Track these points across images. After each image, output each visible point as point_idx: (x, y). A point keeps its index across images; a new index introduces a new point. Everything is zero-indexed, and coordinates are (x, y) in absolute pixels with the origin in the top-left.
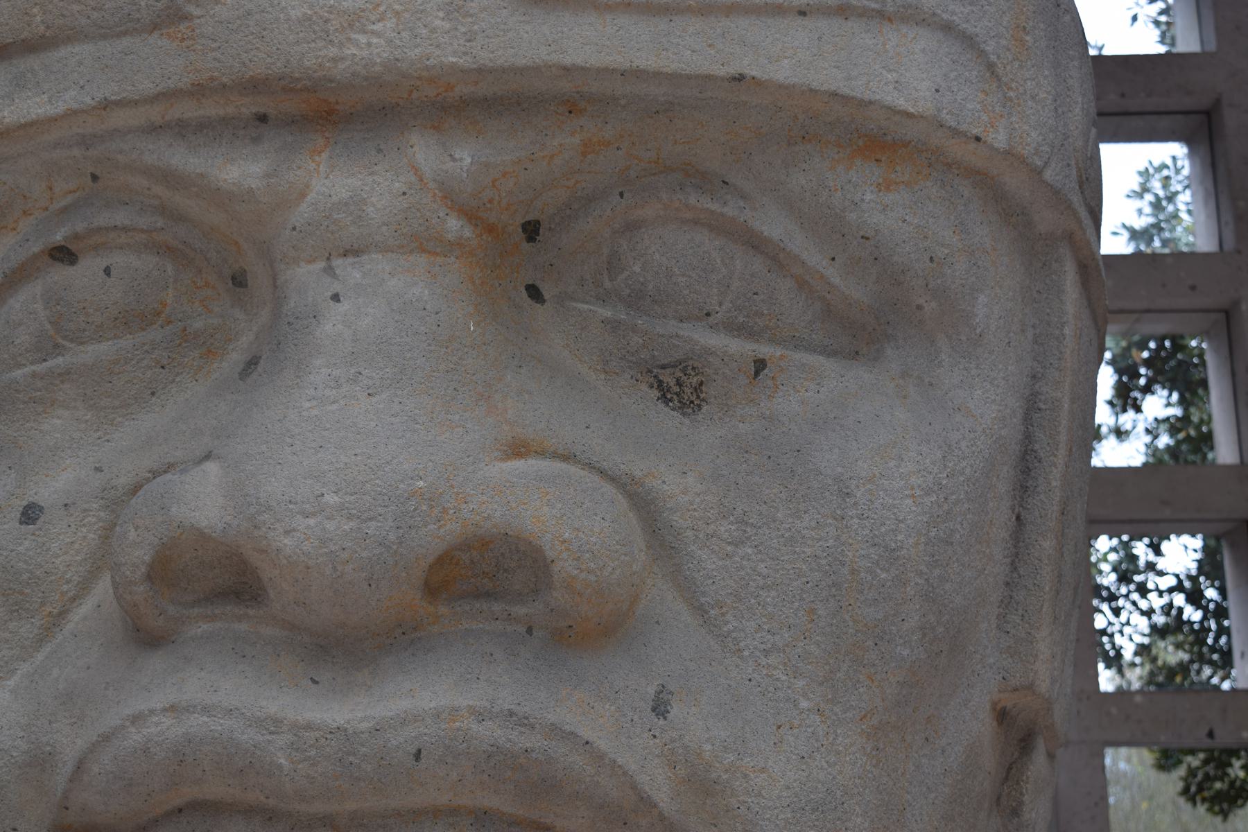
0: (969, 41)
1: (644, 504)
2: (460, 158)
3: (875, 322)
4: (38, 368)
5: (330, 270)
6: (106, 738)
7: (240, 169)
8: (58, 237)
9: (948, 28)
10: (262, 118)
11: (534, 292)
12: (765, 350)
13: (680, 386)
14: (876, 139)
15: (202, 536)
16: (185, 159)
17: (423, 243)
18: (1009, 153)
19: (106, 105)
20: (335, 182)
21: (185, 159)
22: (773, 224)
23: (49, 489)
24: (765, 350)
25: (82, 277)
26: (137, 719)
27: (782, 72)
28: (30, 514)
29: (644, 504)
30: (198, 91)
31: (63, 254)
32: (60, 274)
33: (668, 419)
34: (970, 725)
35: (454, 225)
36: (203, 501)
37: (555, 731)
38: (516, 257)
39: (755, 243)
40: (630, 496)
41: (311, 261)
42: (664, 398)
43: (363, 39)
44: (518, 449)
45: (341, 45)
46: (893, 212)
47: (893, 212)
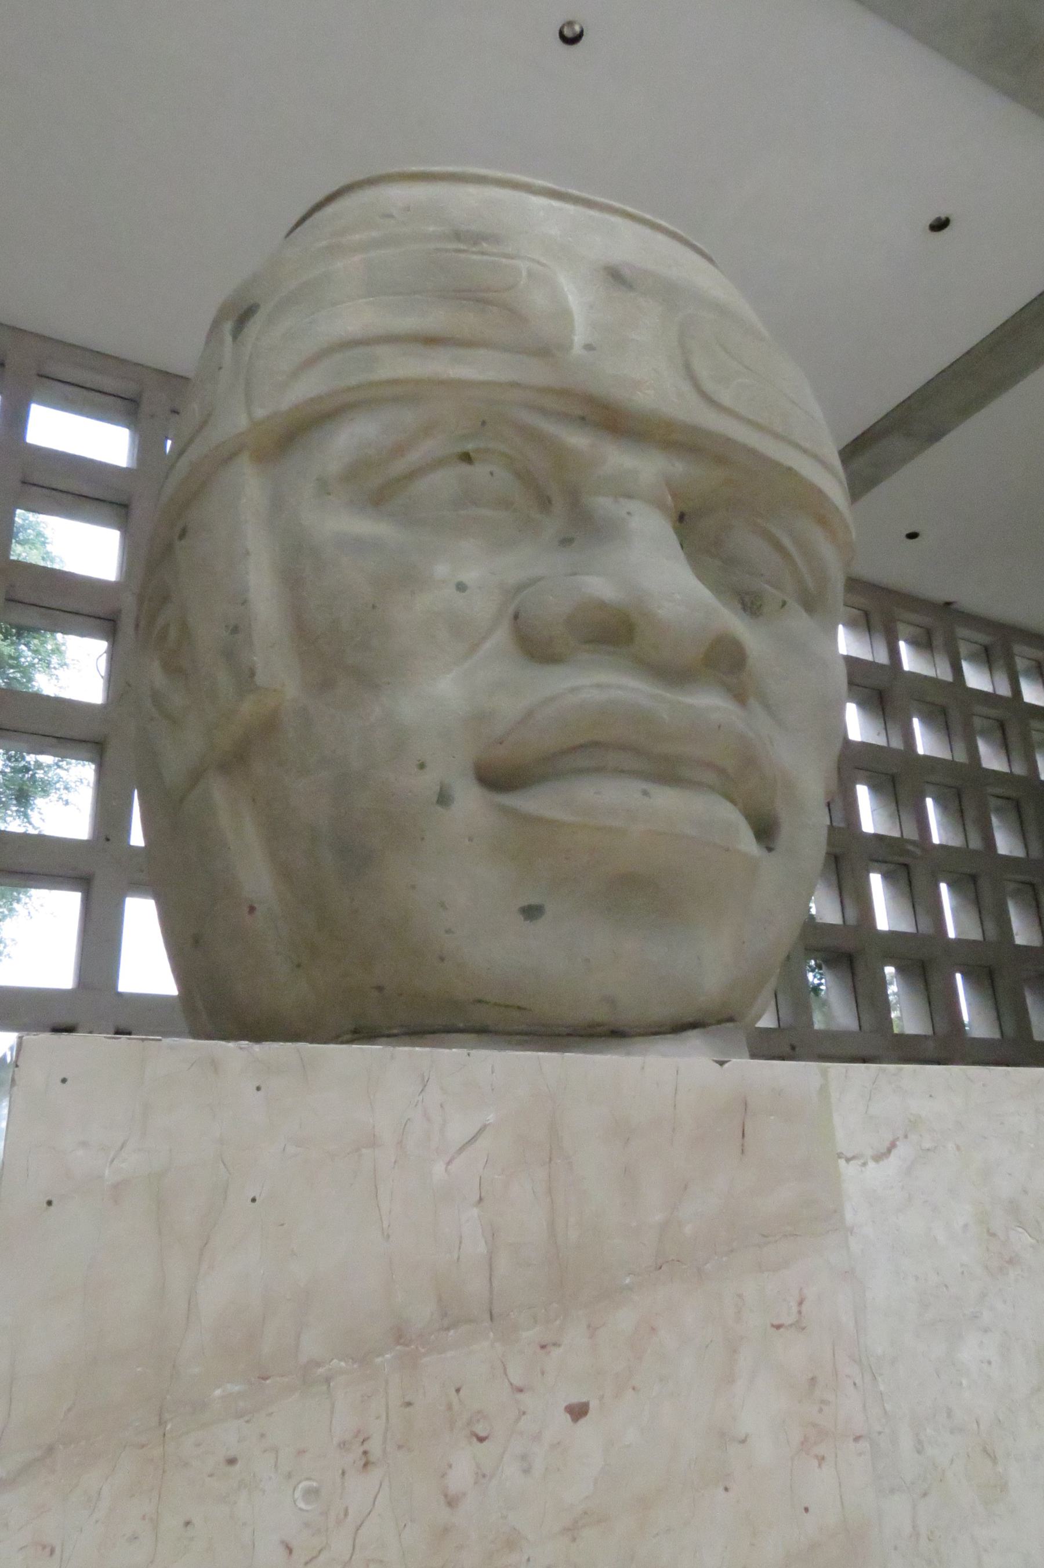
2: (679, 467)
8: (470, 447)
17: (661, 506)
20: (619, 459)
23: (470, 575)
25: (479, 471)
28: (461, 587)
31: (466, 458)
32: (464, 468)
36: (600, 587)
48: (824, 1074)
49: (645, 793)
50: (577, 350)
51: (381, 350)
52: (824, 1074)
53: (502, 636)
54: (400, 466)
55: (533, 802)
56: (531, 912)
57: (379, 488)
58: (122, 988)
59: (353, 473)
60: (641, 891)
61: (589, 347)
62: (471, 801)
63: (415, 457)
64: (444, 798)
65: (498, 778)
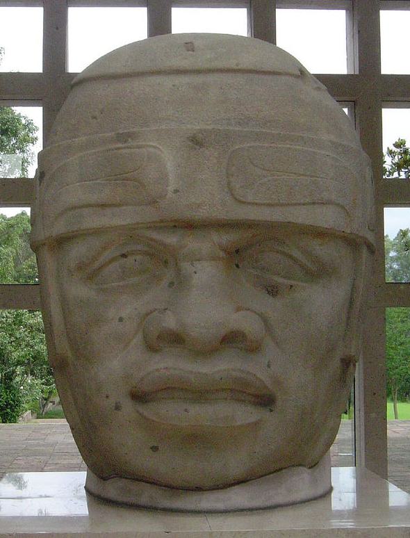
0: (343, 207)
1: (265, 320)
2: (227, 238)
3: (319, 272)
4: (121, 284)
5: (192, 264)
6: (149, 374)
7: (171, 239)
8: (124, 251)
9: (338, 205)
10: (175, 226)
11: (237, 266)
12: (293, 282)
13: (273, 291)
14: (321, 234)
15: (171, 330)
16: (155, 235)
17: (214, 258)
18: (351, 233)
19: (138, 223)
21: (155, 235)
22: (296, 254)
24: (293, 282)
25: (130, 260)
26: (157, 370)
27: (300, 221)
28: (121, 320)
29: (265, 320)
30: (162, 221)
31: (124, 256)
33: (271, 299)
34: (336, 364)
35: (222, 254)
36: (170, 322)
37: (242, 371)
38: (235, 257)
39: (290, 257)
40: (266, 325)
41: (188, 262)
42: (269, 293)
43: (201, 211)
44: (238, 309)
45: (196, 212)
46: (325, 251)
47: (325, 251)
48: (405, 422)
49: (186, 410)
50: (170, 195)
51: (86, 210)
52: (405, 422)
53: (138, 340)
54: (97, 265)
55: (148, 411)
56: (155, 449)
57: (90, 273)
58: (381, 11)
59: (80, 267)
60: (196, 439)
61: (176, 191)
62: (128, 406)
63: (102, 259)
64: (118, 408)
65: (139, 397)
